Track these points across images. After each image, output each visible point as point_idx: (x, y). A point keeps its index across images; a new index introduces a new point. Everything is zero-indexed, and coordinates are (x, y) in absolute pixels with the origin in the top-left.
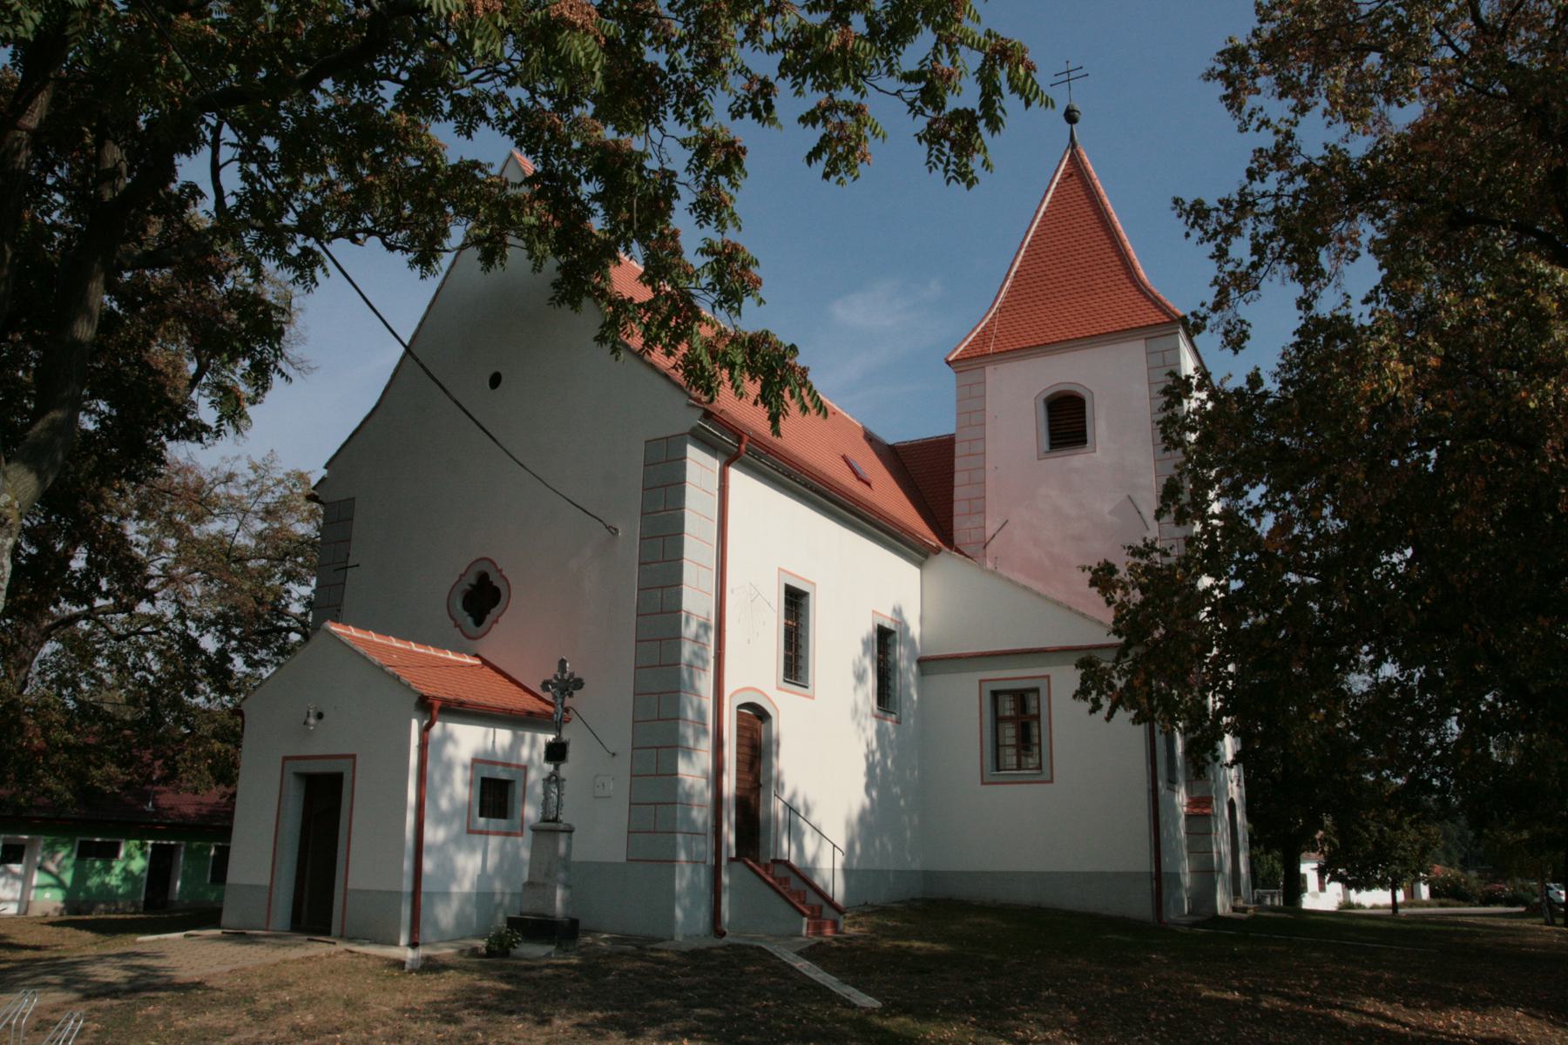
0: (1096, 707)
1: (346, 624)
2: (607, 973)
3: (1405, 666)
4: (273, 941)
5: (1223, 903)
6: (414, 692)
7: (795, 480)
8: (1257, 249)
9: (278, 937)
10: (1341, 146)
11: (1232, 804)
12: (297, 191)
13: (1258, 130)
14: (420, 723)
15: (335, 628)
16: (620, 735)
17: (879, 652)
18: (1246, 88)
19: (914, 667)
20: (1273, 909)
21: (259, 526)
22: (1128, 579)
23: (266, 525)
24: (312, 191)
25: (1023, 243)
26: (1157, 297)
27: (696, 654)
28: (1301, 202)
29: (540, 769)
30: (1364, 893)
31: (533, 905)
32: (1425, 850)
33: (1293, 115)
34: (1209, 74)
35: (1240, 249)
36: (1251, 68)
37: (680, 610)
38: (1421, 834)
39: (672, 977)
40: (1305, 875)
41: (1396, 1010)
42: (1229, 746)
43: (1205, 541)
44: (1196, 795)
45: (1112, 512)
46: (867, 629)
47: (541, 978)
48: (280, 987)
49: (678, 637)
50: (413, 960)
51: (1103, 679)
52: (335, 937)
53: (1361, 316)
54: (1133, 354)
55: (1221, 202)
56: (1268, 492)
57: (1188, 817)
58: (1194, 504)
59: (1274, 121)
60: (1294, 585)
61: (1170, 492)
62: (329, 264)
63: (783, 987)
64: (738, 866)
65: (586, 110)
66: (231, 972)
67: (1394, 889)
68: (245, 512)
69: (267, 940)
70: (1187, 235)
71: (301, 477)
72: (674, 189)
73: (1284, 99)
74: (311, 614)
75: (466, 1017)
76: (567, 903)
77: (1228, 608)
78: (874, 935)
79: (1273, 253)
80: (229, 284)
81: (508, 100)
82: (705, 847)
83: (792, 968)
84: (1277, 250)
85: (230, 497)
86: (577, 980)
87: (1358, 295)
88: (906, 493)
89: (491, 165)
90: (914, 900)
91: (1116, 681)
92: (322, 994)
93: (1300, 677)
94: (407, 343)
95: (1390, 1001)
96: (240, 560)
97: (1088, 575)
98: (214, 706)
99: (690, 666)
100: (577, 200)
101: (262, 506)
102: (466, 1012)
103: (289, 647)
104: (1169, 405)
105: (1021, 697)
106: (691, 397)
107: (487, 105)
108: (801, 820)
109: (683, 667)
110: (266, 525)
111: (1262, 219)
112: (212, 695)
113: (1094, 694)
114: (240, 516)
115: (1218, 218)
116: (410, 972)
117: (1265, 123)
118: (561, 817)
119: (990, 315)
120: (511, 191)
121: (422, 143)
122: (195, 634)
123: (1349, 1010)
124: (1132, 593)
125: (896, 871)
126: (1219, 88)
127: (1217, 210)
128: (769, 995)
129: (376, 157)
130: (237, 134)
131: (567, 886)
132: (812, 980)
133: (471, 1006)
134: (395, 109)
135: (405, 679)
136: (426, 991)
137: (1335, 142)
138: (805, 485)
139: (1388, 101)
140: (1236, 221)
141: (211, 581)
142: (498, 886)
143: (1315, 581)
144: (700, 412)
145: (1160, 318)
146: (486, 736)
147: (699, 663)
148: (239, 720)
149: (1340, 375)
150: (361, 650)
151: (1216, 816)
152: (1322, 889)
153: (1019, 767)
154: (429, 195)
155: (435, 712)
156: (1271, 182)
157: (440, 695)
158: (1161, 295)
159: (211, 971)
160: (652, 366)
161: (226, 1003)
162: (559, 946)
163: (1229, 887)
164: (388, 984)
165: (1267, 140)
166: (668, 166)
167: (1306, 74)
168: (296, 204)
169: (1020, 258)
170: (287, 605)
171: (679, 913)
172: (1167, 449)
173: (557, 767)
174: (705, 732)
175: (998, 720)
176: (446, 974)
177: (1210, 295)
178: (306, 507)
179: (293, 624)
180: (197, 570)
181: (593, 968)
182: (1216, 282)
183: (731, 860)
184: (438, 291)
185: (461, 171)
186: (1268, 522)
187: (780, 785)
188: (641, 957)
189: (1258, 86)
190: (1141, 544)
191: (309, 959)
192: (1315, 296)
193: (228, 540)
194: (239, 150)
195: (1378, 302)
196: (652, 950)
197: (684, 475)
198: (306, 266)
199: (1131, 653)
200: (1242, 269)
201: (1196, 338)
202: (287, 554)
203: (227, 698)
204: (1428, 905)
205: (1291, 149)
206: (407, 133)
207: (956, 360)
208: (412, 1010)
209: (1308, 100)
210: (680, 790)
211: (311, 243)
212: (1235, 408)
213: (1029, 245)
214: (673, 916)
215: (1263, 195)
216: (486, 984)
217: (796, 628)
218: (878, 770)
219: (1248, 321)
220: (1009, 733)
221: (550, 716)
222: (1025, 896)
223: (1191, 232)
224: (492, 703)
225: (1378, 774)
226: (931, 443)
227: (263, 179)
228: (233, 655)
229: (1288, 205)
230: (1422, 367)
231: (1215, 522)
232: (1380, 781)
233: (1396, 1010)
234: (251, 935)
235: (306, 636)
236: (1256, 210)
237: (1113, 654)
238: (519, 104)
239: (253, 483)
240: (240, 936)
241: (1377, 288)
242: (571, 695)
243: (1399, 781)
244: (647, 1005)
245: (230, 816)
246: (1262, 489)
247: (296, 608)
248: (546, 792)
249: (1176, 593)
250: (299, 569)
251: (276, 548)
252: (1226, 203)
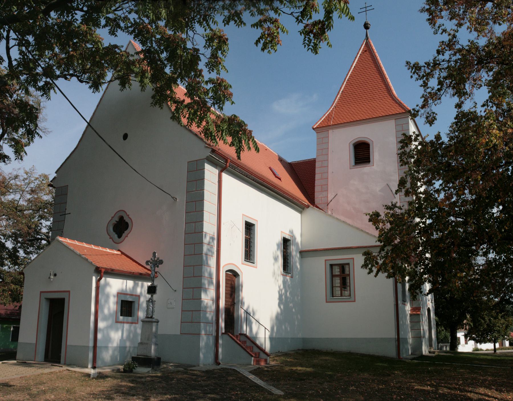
0: (371, 271)
1: (65, 237)
2: (172, 379)
3: (498, 253)
4: (38, 365)
5: (425, 350)
6: (94, 265)
7: (249, 178)
8: (440, 83)
9: (39, 364)
10: (475, 41)
11: (429, 310)
12: (42, 58)
13: (442, 34)
14: (96, 278)
15: (61, 239)
16: (178, 283)
17: (284, 248)
18: (437, 16)
19: (298, 255)
20: (446, 352)
21: (29, 196)
22: (384, 219)
23: (31, 196)
24: (49, 58)
25: (345, 79)
26: (400, 102)
27: (208, 250)
28: (458, 64)
29: (145, 296)
30: (483, 344)
31: (141, 352)
32: (507, 327)
33: (456, 27)
34: (422, 10)
35: (433, 83)
36: (439, 7)
37: (202, 232)
38: (505, 320)
39: (198, 381)
40: (459, 338)
41: (492, 392)
42: (427, 286)
43: (417, 203)
44: (414, 306)
45: (380, 191)
46: (279, 239)
47: (146, 381)
48: (40, 384)
49: (201, 243)
50: (94, 374)
51: (374, 260)
52: (62, 364)
53: (481, 111)
54: (390, 125)
55: (426, 63)
56: (443, 183)
57: (411, 315)
58: (412, 187)
59: (448, 30)
60: (453, 222)
61: (402, 183)
62: (56, 88)
63: (244, 386)
64: (226, 336)
65: (161, 24)
66: (20, 378)
67: (495, 343)
68: (23, 191)
69: (34, 365)
70: (412, 77)
71: (46, 177)
72: (198, 56)
73: (452, 21)
74: (51, 233)
75: (115, 397)
76: (156, 350)
77: (426, 231)
78: (282, 365)
79: (447, 85)
80: (15, 96)
81: (129, 19)
82: (212, 329)
83: (247, 378)
84: (448, 83)
85: (17, 185)
86: (160, 382)
87: (480, 103)
88: (295, 183)
89: (122, 46)
90: (299, 350)
91: (379, 261)
92: (57, 387)
93: (455, 259)
94: (88, 121)
95: (491, 389)
96: (20, 211)
97: (368, 217)
98: (11, 270)
99: (206, 255)
100: (160, 60)
101: (30, 189)
102: (115, 395)
103: (41, 246)
104: (402, 147)
105: (343, 267)
106: (206, 144)
107: (120, 22)
108: (251, 317)
109: (204, 255)
110: (31, 196)
111: (443, 70)
112: (11, 266)
113: (370, 266)
114: (21, 193)
115: (425, 70)
116: (93, 378)
117: (444, 31)
118: (154, 316)
119: (331, 109)
120: (131, 58)
121: (93, 37)
122: (3, 241)
123: (474, 393)
124: (386, 224)
125: (291, 338)
126: (426, 15)
127: (424, 67)
128: (238, 389)
129: (74, 44)
130: (16, 35)
131: (156, 344)
132: (256, 383)
133: (118, 392)
134: (81, 23)
135: (90, 260)
136: (99, 386)
137: (473, 39)
138: (253, 180)
139: (495, 22)
140: (431, 71)
141: (10, 219)
142: (128, 344)
143: (461, 220)
144: (210, 150)
145: (400, 110)
146: (123, 283)
147: (210, 254)
148: (22, 276)
149: (472, 136)
150: (72, 248)
151: (422, 315)
152: (466, 343)
153: (341, 295)
154: (97, 59)
155: (102, 274)
156: (447, 55)
157: (104, 267)
158: (402, 101)
159: (13, 377)
160: (190, 131)
161: (19, 390)
162: (153, 368)
163: (428, 343)
164: (84, 383)
165: (446, 38)
166: (196, 47)
167: (462, 10)
168: (41, 64)
169: (344, 86)
170: (41, 229)
171: (201, 355)
172: (402, 165)
173: (152, 296)
174: (212, 283)
175: (333, 276)
176: (107, 379)
177: (421, 102)
178: (47, 190)
179: (43, 237)
180: (4, 215)
181: (166, 377)
182: (423, 96)
183: (223, 334)
184: (101, 100)
185: (110, 49)
186: (442, 196)
187: (243, 303)
188: (186, 373)
189: (442, 15)
190: (390, 205)
191: (51, 373)
192: (462, 102)
193: (16, 202)
194: (17, 41)
195: (488, 106)
196: (191, 370)
197: (204, 176)
198: (46, 89)
199: (386, 249)
200: (434, 91)
201: (416, 119)
202: (40, 208)
203: (17, 267)
204: (509, 349)
205: (455, 42)
206: (87, 34)
207: (317, 128)
208: (94, 394)
209: (462, 22)
210: (202, 305)
211: (48, 80)
212: (430, 149)
213: (348, 80)
214: (199, 356)
215: (443, 61)
216: (123, 384)
218: (283, 297)
219: (436, 112)
220: (337, 282)
221: (149, 275)
222: (344, 348)
223: (413, 76)
224: (125, 270)
225: (488, 297)
226: (307, 162)
227: (28, 54)
228: (19, 250)
229: (453, 65)
230: (506, 134)
231: (421, 195)
232: (489, 300)
233: (492, 392)
234: (28, 363)
235: (49, 243)
236: (440, 67)
237: (378, 249)
238: (134, 21)
239: (26, 179)
240: (24, 364)
241: (487, 100)
242: (158, 267)
243: (496, 300)
244: (189, 392)
245: (19, 314)
246: (441, 182)
247: (44, 230)
248: (148, 306)
249: (404, 225)
250: (45, 214)
251: (36, 206)
252: (428, 64)
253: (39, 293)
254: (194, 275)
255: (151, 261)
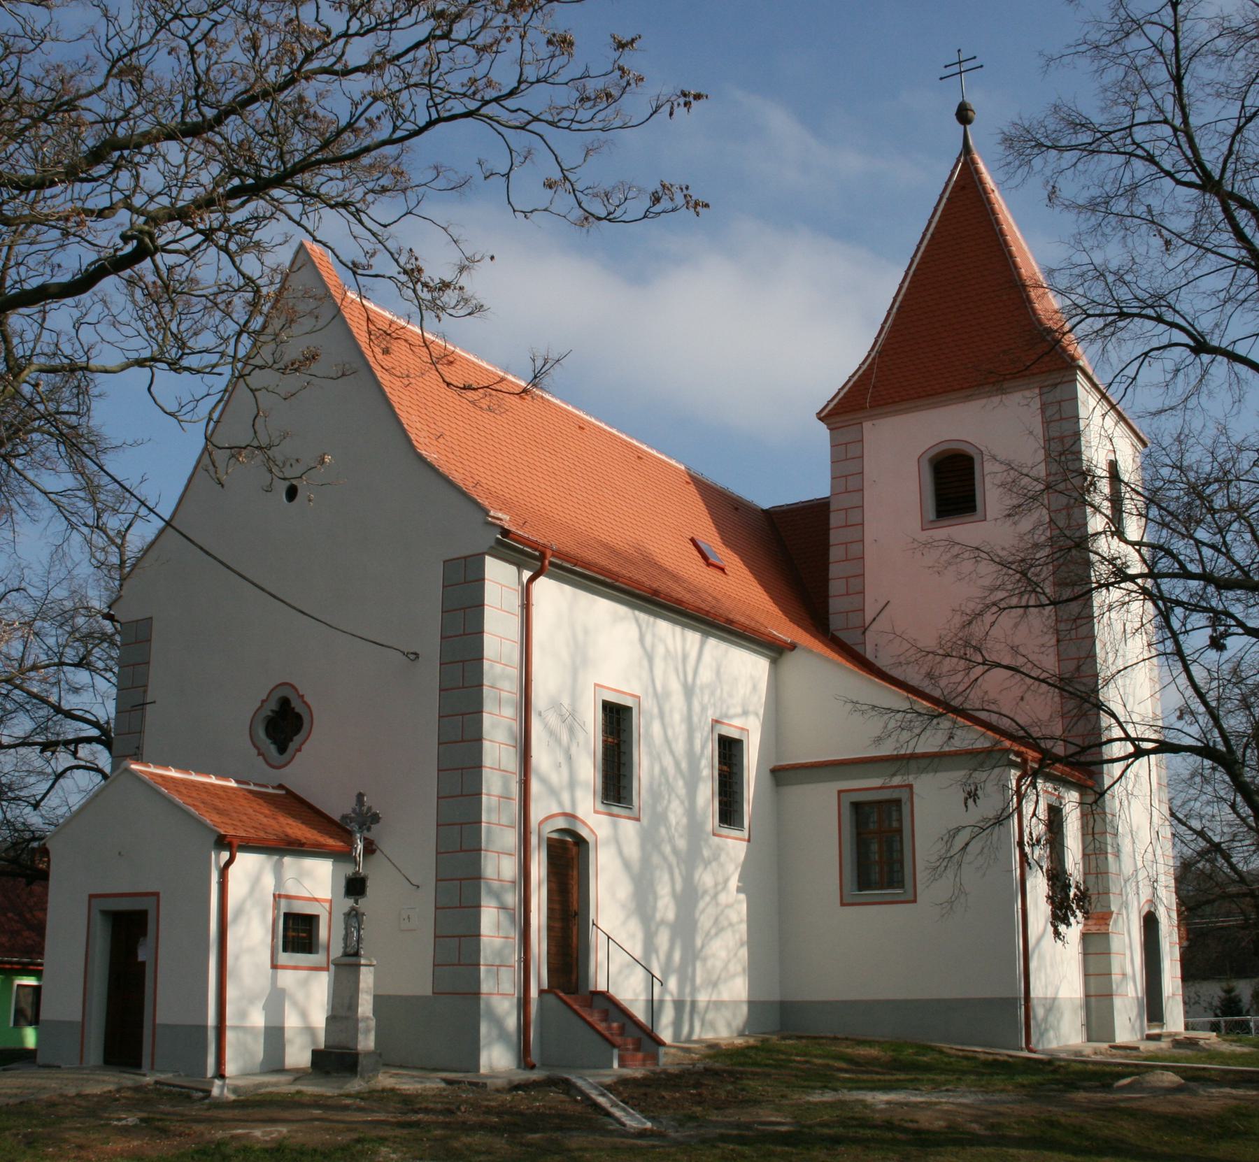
1: (145, 764)
16: (424, 870)
64: (551, 999)
207: (826, 416)
217: (618, 745)
242: (369, 829)
253: (86, 898)
254: (464, 848)
255: (353, 815)
